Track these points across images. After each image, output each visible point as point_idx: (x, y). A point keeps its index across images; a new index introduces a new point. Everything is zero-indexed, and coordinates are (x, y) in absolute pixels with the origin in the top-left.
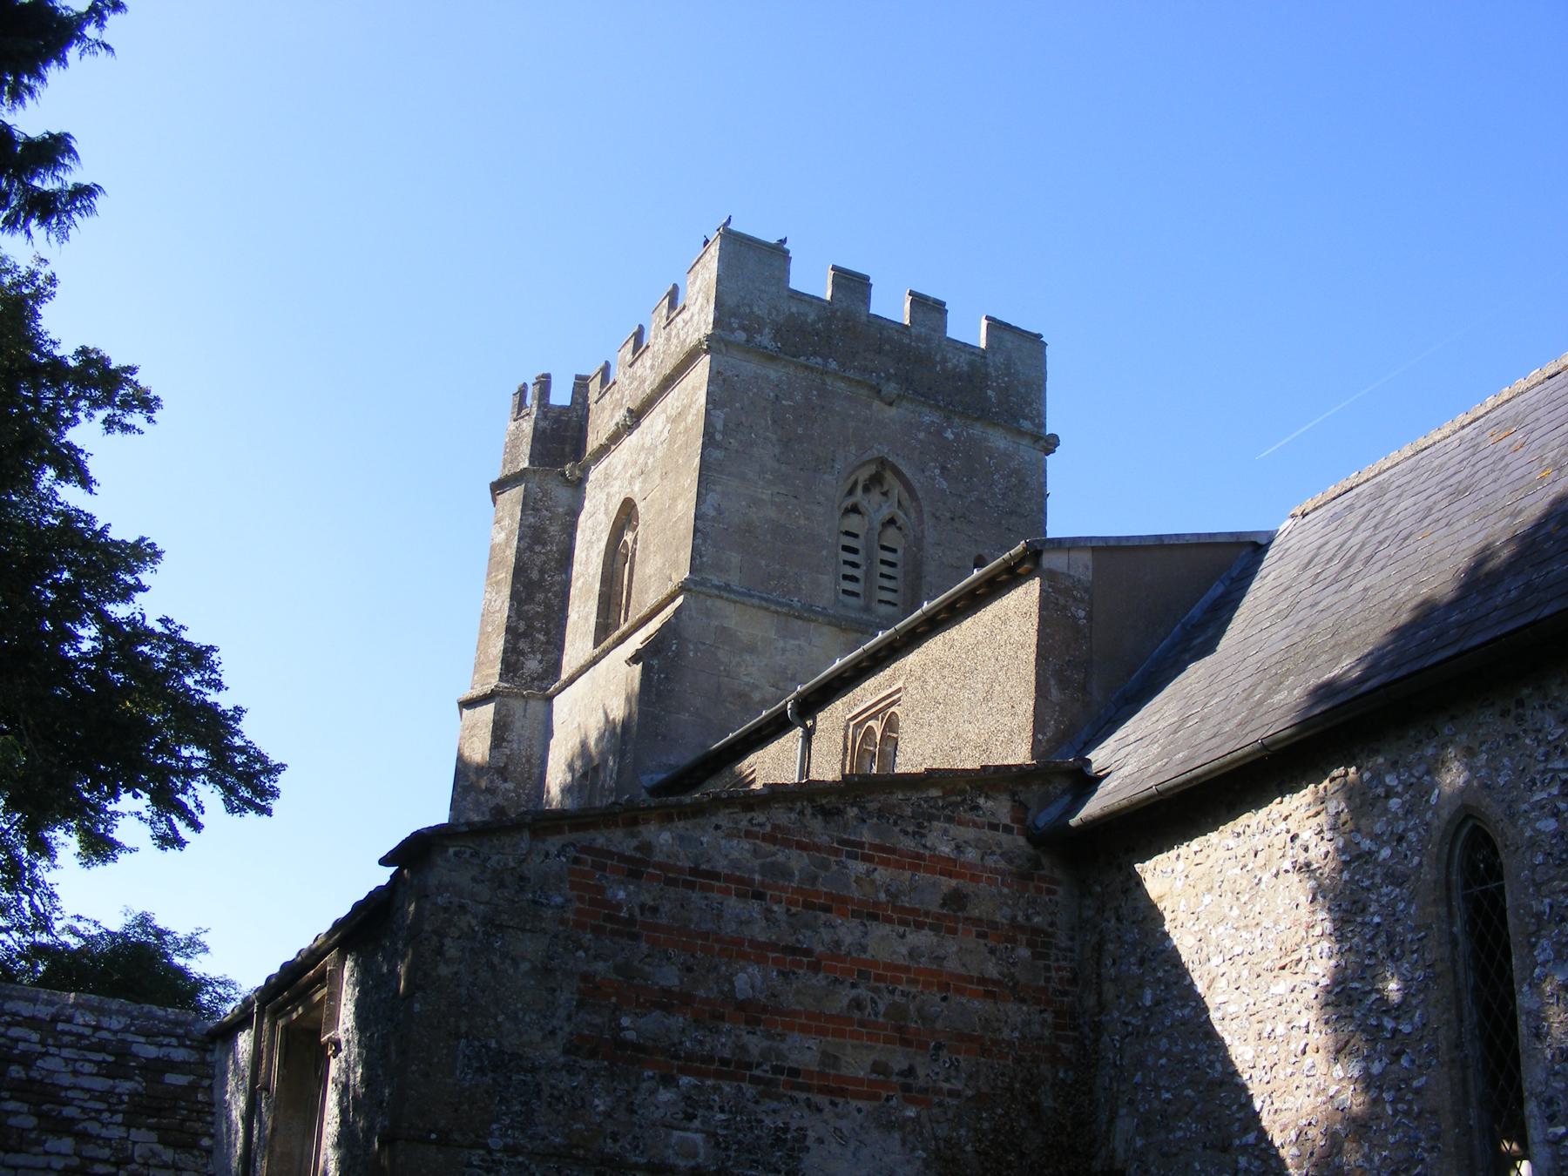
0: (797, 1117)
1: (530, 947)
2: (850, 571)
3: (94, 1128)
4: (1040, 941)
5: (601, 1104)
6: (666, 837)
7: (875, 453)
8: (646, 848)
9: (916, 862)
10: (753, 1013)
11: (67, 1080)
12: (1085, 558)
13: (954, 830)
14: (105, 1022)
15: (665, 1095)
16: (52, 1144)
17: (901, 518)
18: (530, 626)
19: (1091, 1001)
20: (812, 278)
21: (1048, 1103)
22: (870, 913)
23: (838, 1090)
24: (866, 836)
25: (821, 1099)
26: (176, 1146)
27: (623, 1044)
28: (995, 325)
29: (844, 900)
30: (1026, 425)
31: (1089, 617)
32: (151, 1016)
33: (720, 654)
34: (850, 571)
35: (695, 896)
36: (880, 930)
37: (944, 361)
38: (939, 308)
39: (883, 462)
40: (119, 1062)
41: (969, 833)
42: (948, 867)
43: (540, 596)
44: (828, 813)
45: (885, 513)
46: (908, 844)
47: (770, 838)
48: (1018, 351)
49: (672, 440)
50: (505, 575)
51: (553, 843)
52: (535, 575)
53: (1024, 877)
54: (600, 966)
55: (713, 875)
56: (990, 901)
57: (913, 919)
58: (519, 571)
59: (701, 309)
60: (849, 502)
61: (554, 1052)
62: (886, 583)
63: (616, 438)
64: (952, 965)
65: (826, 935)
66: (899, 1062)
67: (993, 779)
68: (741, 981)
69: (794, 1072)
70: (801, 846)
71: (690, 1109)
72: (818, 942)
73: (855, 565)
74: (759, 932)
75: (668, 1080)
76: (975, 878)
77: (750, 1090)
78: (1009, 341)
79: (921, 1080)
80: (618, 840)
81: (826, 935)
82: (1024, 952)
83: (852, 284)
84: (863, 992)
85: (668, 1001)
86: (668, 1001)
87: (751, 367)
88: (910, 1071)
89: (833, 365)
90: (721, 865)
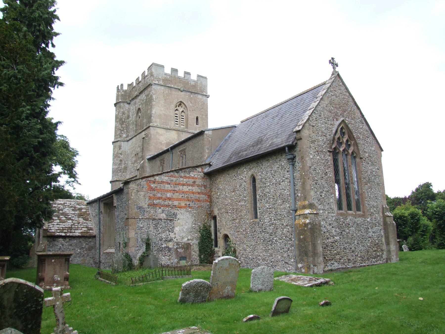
2: (177, 120)
3: (73, 218)
4: (205, 187)
5: (152, 212)
8: (155, 179)
10: (170, 199)
11: (68, 212)
13: (194, 173)
14: (71, 203)
15: (160, 210)
16: (69, 221)
22: (183, 185)
23: (181, 207)
25: (179, 209)
26: (86, 220)
27: (154, 204)
28: (199, 76)
31: (212, 140)
32: (78, 202)
34: (177, 120)
35: (162, 185)
36: (185, 187)
38: (189, 74)
39: (181, 102)
40: (75, 209)
41: (196, 173)
43: (125, 124)
45: (182, 110)
46: (188, 175)
49: (146, 100)
51: (144, 180)
52: (123, 120)
53: (203, 178)
56: (199, 182)
57: (189, 185)
60: (176, 108)
64: (194, 191)
65: (178, 188)
70: (174, 177)
74: (170, 189)
75: (160, 208)
77: (170, 208)
79: (191, 205)
80: (152, 179)
81: (178, 188)
82: (203, 188)
83: (174, 71)
84: (183, 195)
85: (159, 198)
86: (159, 198)
88: (189, 204)
90: (164, 181)
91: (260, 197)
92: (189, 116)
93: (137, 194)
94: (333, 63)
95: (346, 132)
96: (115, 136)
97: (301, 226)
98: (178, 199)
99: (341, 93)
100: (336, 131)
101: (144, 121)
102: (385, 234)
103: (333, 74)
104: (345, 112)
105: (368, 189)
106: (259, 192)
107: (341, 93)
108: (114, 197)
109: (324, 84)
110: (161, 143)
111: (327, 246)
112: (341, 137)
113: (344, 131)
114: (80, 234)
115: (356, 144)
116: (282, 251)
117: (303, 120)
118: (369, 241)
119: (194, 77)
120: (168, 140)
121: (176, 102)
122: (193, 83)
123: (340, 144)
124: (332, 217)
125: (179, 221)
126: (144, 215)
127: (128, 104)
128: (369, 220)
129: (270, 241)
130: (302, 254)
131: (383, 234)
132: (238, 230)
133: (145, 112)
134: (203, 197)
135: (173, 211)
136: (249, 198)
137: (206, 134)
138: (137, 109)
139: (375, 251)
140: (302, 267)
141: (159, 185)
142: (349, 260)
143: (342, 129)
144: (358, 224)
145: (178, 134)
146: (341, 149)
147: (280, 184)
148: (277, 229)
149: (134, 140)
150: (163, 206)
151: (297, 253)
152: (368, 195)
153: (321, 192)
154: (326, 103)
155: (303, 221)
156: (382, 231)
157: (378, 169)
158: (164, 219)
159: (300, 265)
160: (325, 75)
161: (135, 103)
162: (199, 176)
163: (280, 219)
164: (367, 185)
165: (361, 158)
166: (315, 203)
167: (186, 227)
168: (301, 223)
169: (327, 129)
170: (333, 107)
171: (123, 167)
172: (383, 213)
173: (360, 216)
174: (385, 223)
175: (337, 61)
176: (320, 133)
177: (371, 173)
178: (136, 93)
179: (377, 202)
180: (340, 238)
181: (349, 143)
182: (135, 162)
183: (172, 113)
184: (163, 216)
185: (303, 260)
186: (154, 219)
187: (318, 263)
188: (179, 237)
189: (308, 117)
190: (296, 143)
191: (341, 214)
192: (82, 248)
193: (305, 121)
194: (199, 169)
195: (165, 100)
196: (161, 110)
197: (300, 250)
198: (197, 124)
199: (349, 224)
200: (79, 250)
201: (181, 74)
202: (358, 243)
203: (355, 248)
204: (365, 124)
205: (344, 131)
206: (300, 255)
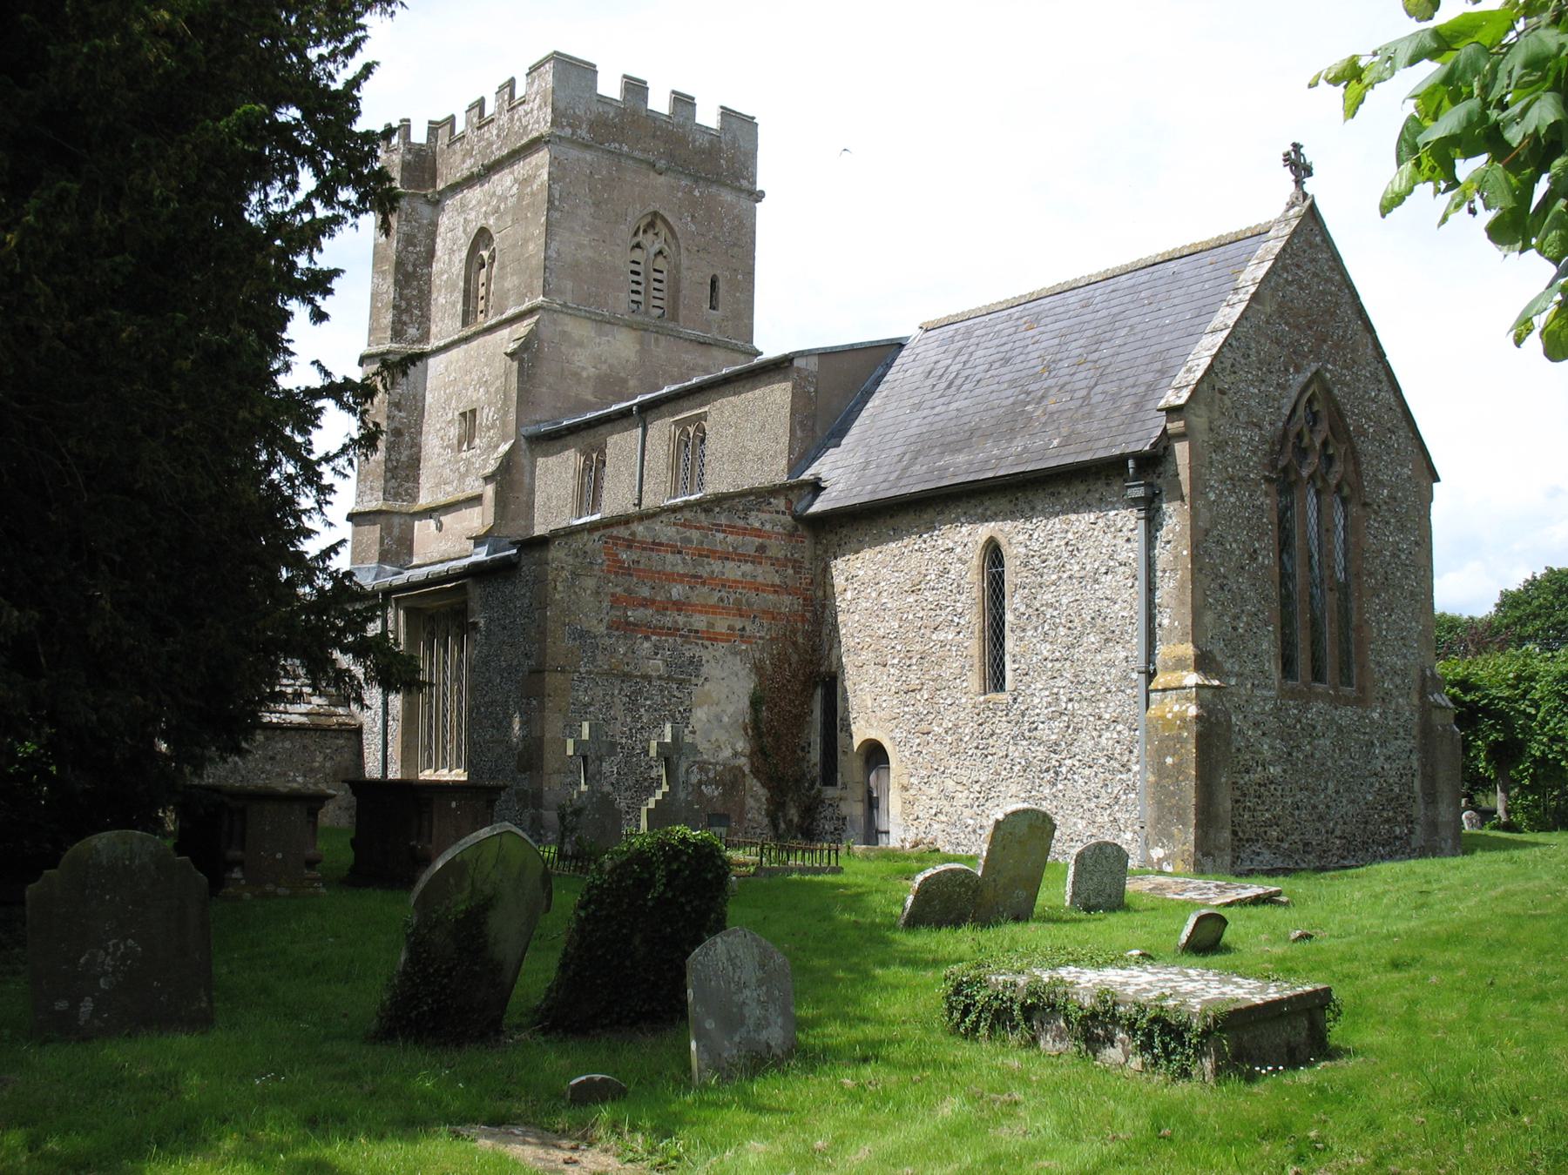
0: (697, 651)
1: (590, 583)
2: (635, 287)
4: (797, 566)
6: (641, 528)
7: (651, 209)
8: (633, 534)
9: (744, 532)
10: (679, 606)
12: (815, 359)
15: (646, 645)
17: (667, 251)
18: (408, 304)
19: (820, 594)
20: (609, 86)
21: (800, 640)
22: (726, 557)
24: (723, 521)
25: (707, 643)
27: (628, 623)
29: (715, 552)
30: (744, 183)
33: (563, 348)
34: (635, 287)
37: (694, 141)
39: (655, 214)
42: (758, 533)
44: (707, 511)
45: (657, 247)
46: (741, 523)
47: (684, 525)
48: (739, 126)
49: (520, 197)
50: (388, 267)
51: (596, 535)
52: (410, 268)
53: (791, 535)
54: (618, 589)
55: (661, 544)
56: (777, 549)
57: (743, 558)
58: (399, 265)
59: (540, 107)
61: (602, 629)
62: (657, 294)
63: (470, 181)
64: (760, 579)
65: (708, 569)
66: (739, 625)
67: (775, 491)
68: (674, 592)
69: (697, 632)
70: (697, 528)
71: (657, 649)
72: (704, 572)
73: (638, 283)
74: (680, 569)
75: (647, 638)
76: (769, 537)
78: (735, 124)
79: (748, 633)
80: (622, 532)
81: (708, 569)
82: (790, 571)
84: (723, 594)
85: (646, 603)
86: (646, 603)
87: (574, 153)
88: (743, 629)
89: (625, 148)
90: (664, 540)
91: (1018, 617)
92: (684, 273)
93: (573, 585)
94: (1299, 166)
95: (1324, 414)
96: (372, 331)
97: (1167, 724)
98: (704, 609)
99: (1315, 275)
100: (1294, 410)
101: (508, 285)
102: (1424, 766)
103: (1292, 205)
104: (1325, 341)
105: (1381, 611)
106: (1014, 604)
107: (1315, 275)
108: (470, 588)
109: (1260, 233)
110: (576, 375)
111: (1244, 795)
112: (1306, 430)
113: (1316, 407)
114: (303, 719)
115: (1354, 456)
116: (1092, 805)
117: (1189, 371)
118: (1372, 785)
119: (707, 117)
120: (604, 367)
121: (636, 214)
122: (703, 141)
123: (1302, 453)
124: (1265, 699)
125: (707, 686)
126: (595, 660)
127: (428, 202)
128: (1376, 715)
129: (1047, 770)
130: (1169, 817)
131: (1416, 765)
132: (924, 726)
133: (514, 246)
134: (787, 603)
135: (690, 651)
136: (973, 619)
137: (799, 370)
138: (473, 229)
139: (1388, 821)
140: (1166, 858)
141: (645, 554)
142: (1306, 844)
143: (1310, 401)
144: (1340, 730)
145: (641, 343)
146: (1305, 473)
147: (1096, 581)
148: (1077, 730)
149: (454, 353)
150: (659, 630)
151: (1150, 813)
152: (1380, 631)
153: (1236, 617)
154: (1268, 310)
155: (1176, 708)
156: (1414, 757)
157: (1417, 544)
158: (660, 678)
159: (1157, 853)
160: (1267, 202)
161: (463, 207)
162: (778, 529)
163: (1090, 700)
164: (1378, 596)
165: (1365, 505)
166: (1216, 652)
167: (731, 709)
168: (1169, 716)
169: (1267, 399)
170: (1287, 324)
171: (404, 458)
172: (1423, 695)
173: (1348, 702)
174: (1427, 730)
175: (1309, 155)
176: (1243, 417)
177: (1393, 555)
178: (469, 162)
179: (1405, 657)
180: (1285, 771)
181: (1331, 451)
182: (460, 444)
183: (621, 258)
184: (657, 666)
185: (1170, 837)
186: (626, 677)
187: (1217, 848)
188: (707, 745)
189: (1208, 360)
190: (1166, 448)
191: (1293, 694)
192: (312, 770)
193: (1199, 374)
194: (780, 503)
195: (597, 205)
196: (580, 246)
197: (1160, 802)
198: (713, 307)
199: (1314, 728)
200: (300, 779)
201: (659, 102)
202: (1337, 792)
203: (1328, 807)
204: (1385, 386)
205: (1316, 407)
206: (1158, 820)
